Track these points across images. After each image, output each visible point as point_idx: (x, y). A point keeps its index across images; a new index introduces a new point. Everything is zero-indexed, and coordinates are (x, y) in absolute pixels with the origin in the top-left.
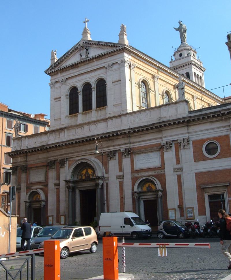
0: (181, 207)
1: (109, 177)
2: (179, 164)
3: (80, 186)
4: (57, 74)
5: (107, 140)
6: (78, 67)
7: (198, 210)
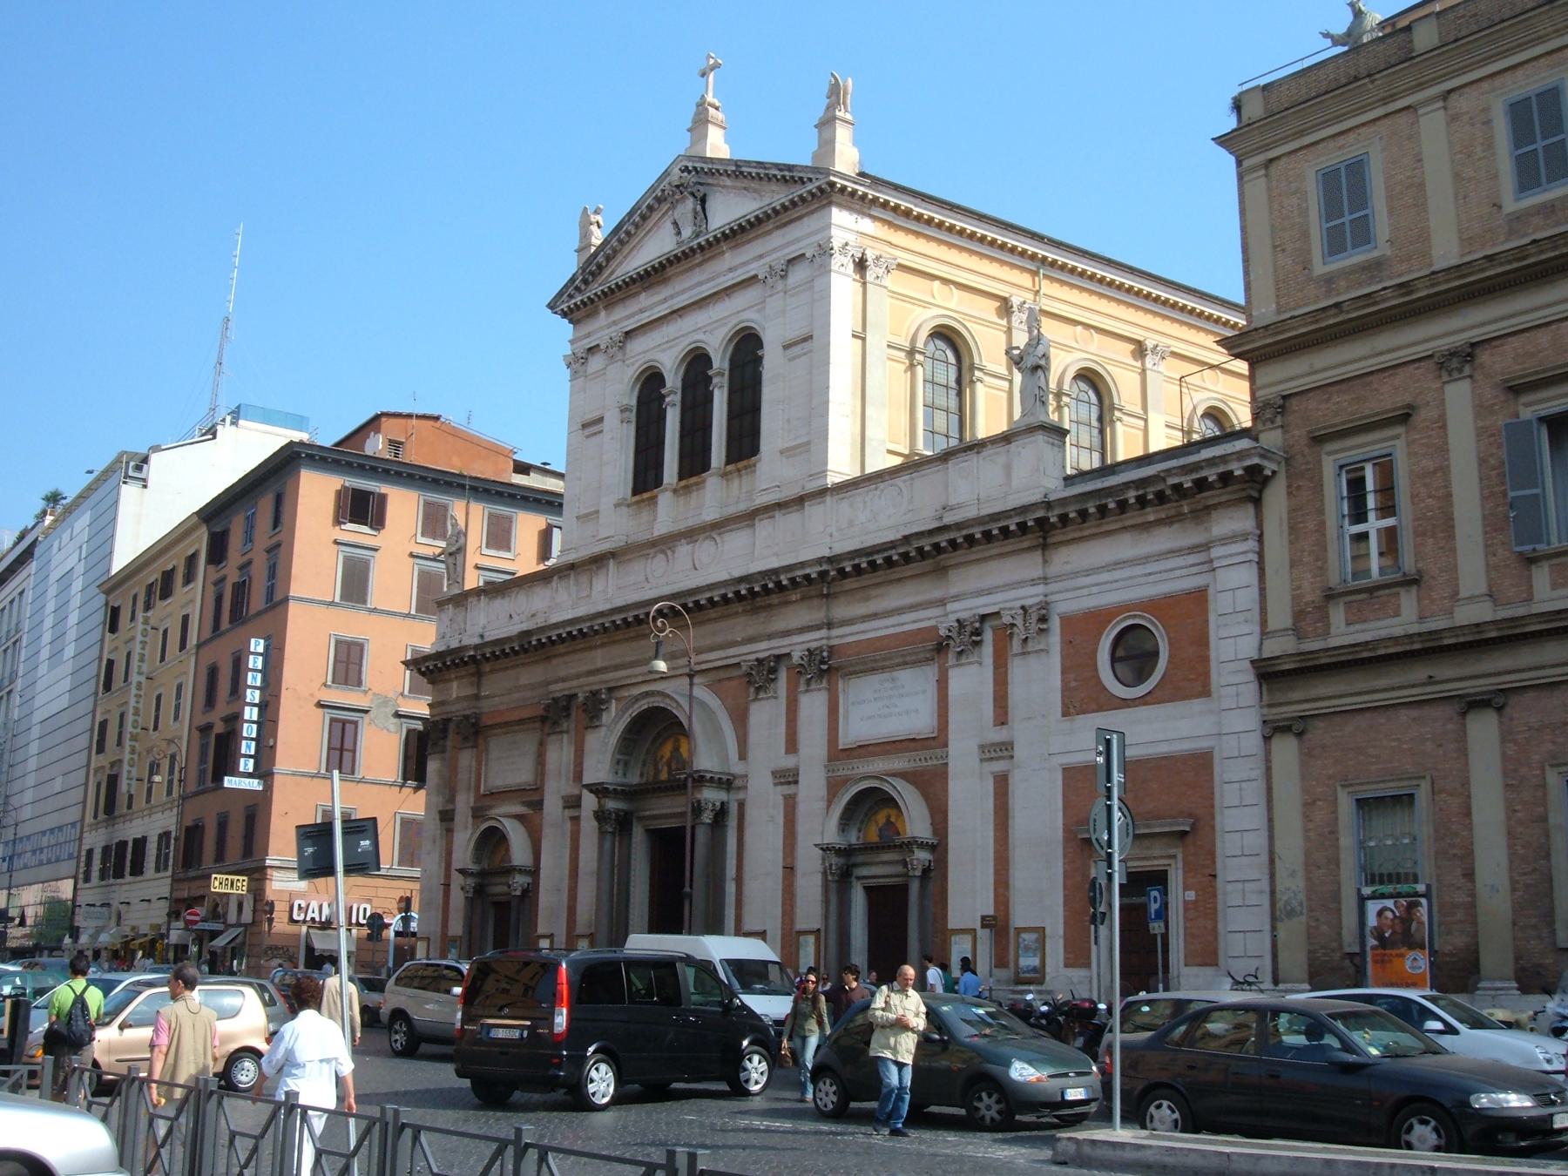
0: (997, 924)
2: (1003, 724)
3: (648, 813)
6: (665, 281)
7: (1061, 942)
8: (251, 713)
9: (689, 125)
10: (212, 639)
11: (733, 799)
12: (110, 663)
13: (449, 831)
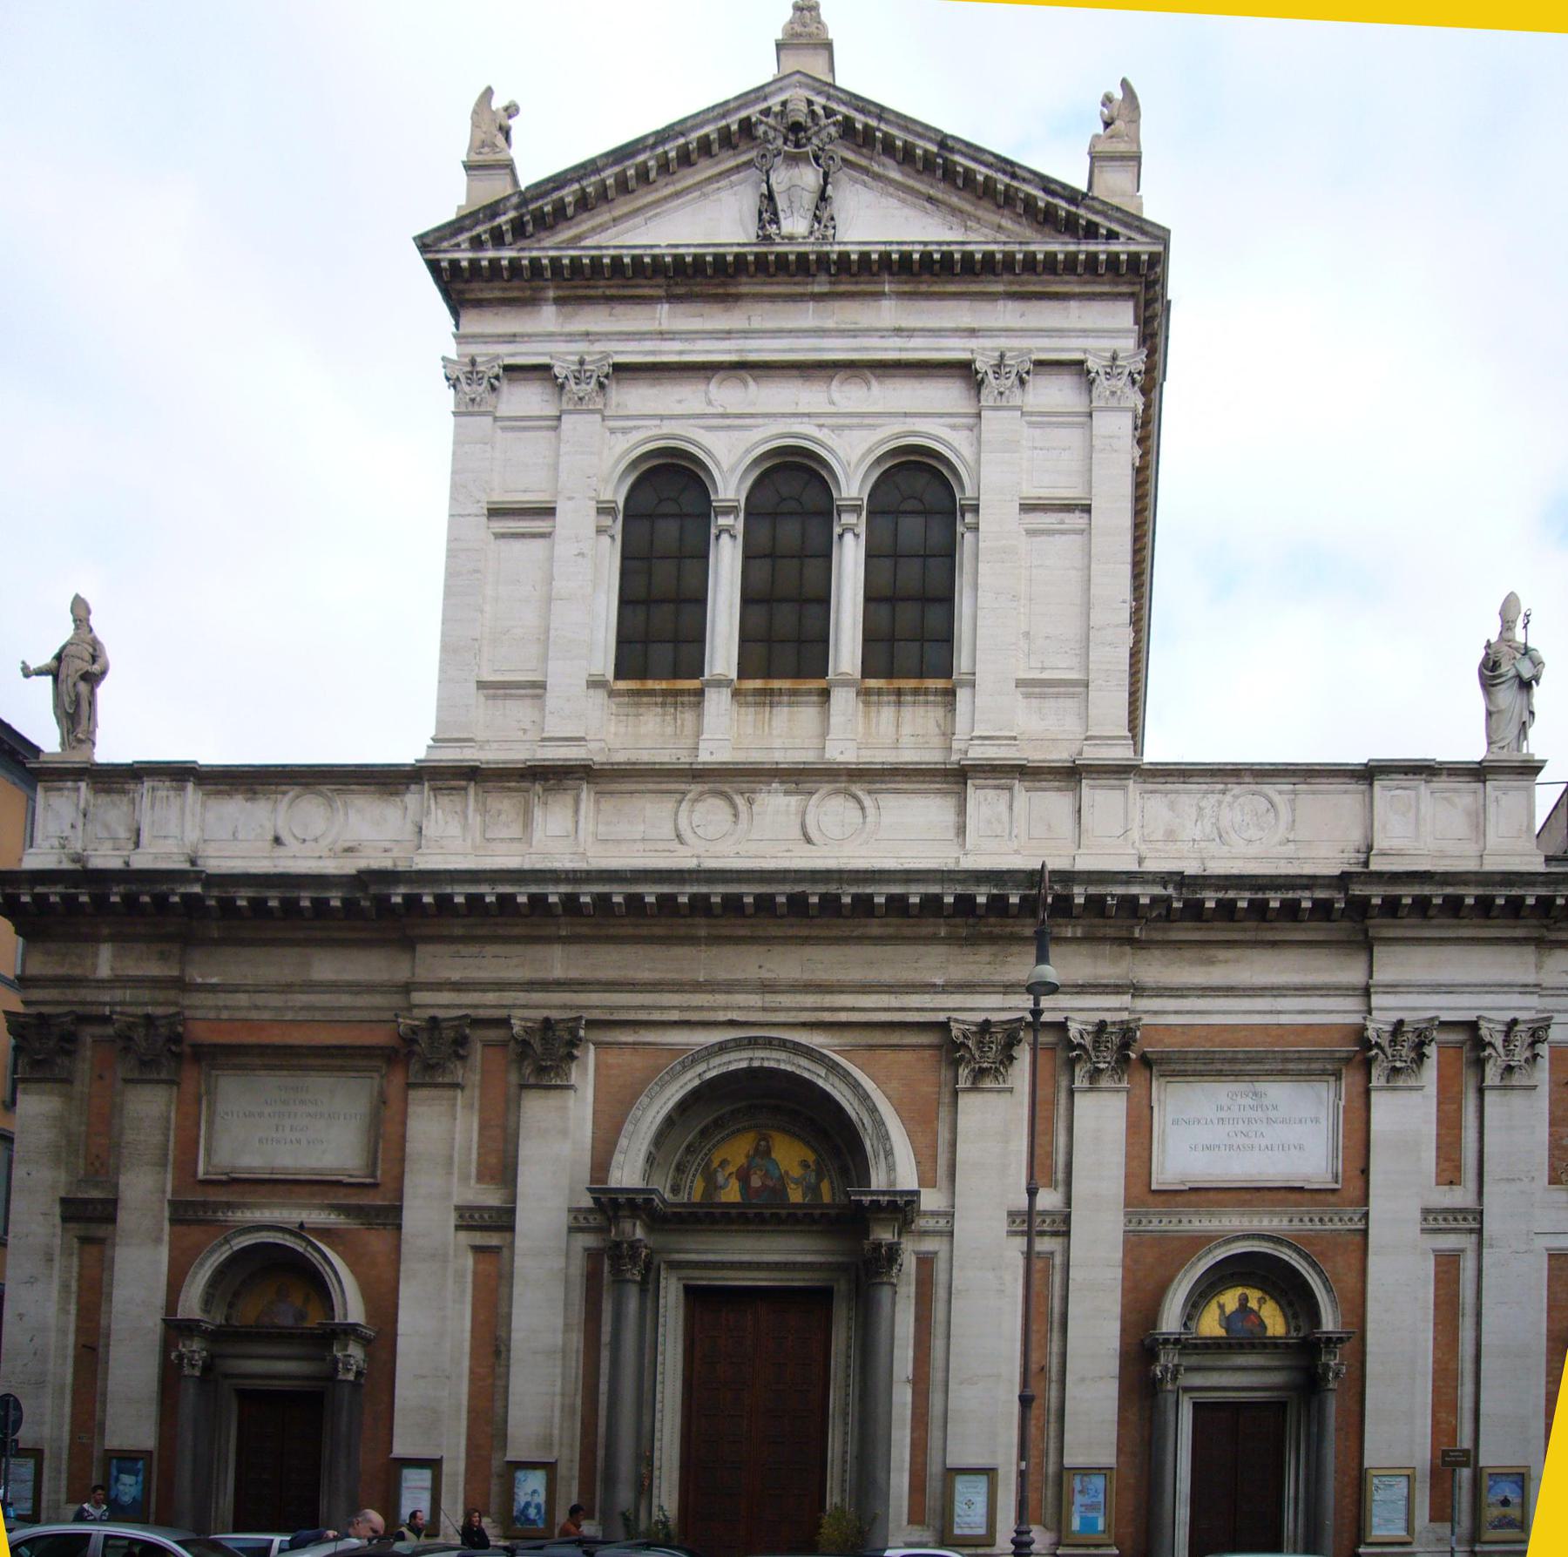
1: (950, 1215)
4: (530, 301)
5: (964, 932)
6: (728, 299)
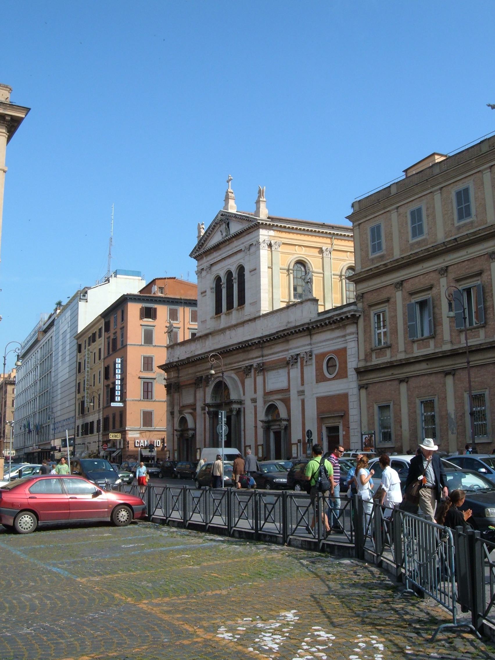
6: (220, 249)
8: (118, 382)
9: (224, 199)
10: (107, 357)
11: (241, 407)
12: (80, 363)
13: (173, 418)
